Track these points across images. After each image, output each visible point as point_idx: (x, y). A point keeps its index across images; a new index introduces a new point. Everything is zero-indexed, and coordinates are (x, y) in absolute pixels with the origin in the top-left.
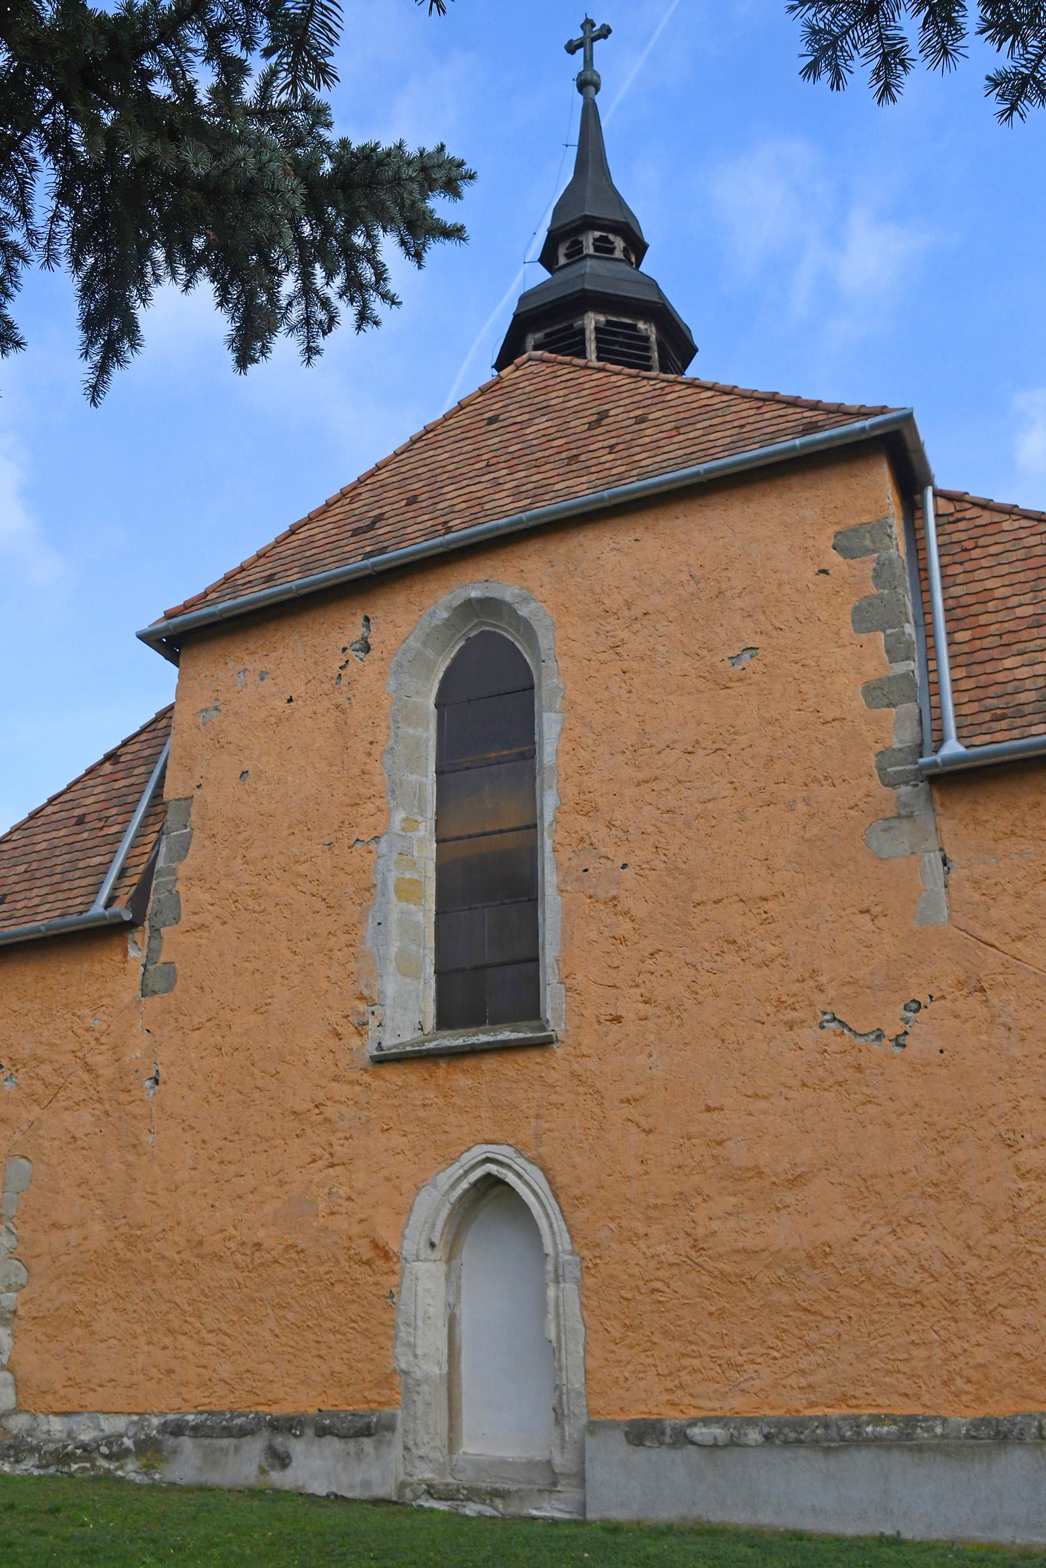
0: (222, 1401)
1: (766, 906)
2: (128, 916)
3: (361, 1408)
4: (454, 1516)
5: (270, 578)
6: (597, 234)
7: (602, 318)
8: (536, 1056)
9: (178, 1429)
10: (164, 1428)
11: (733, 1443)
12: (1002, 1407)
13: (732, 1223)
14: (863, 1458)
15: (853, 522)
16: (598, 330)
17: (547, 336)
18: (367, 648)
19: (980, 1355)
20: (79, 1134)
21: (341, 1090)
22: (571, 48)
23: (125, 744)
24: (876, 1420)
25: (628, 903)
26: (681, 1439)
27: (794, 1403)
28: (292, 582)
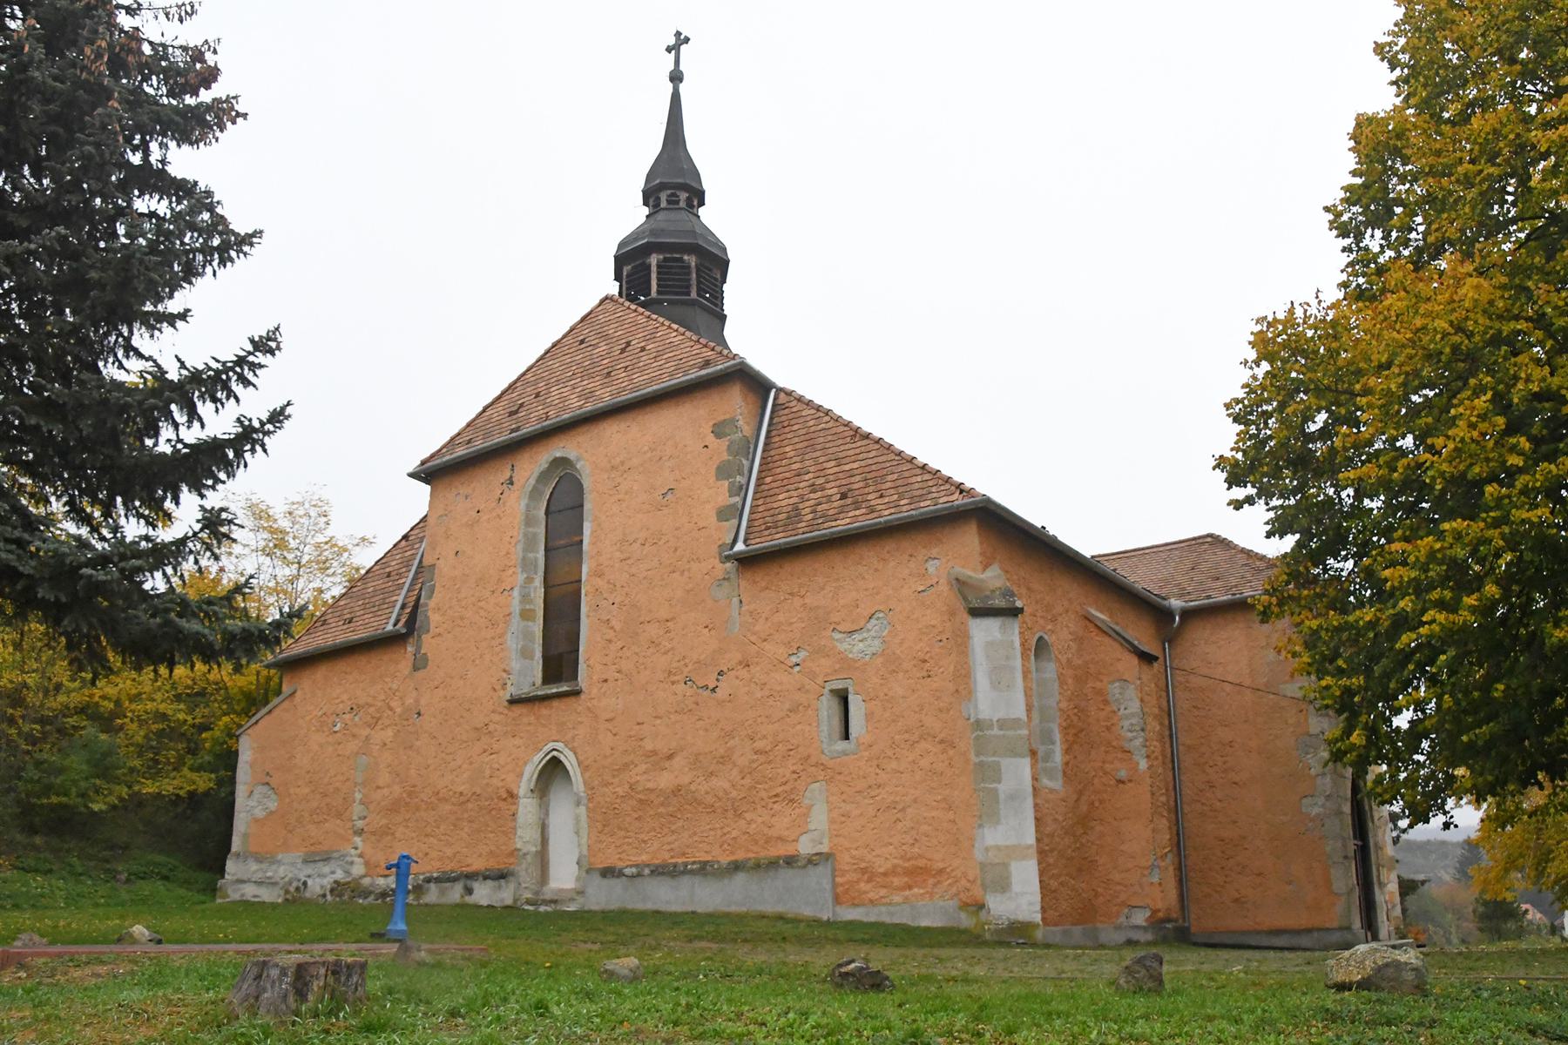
0: (449, 866)
1: (669, 624)
2: (404, 631)
3: (502, 866)
4: (537, 913)
5: (469, 442)
6: (669, 192)
7: (661, 257)
8: (571, 700)
9: (428, 880)
10: (424, 881)
11: (639, 875)
12: (740, 855)
13: (645, 776)
14: (686, 880)
15: (722, 418)
16: (658, 266)
17: (665, 259)
18: (512, 483)
19: (734, 834)
20: (387, 742)
21: (496, 717)
22: (669, 50)
23: (412, 529)
24: (694, 863)
25: (614, 623)
26: (621, 874)
27: (665, 857)
28: (479, 444)
